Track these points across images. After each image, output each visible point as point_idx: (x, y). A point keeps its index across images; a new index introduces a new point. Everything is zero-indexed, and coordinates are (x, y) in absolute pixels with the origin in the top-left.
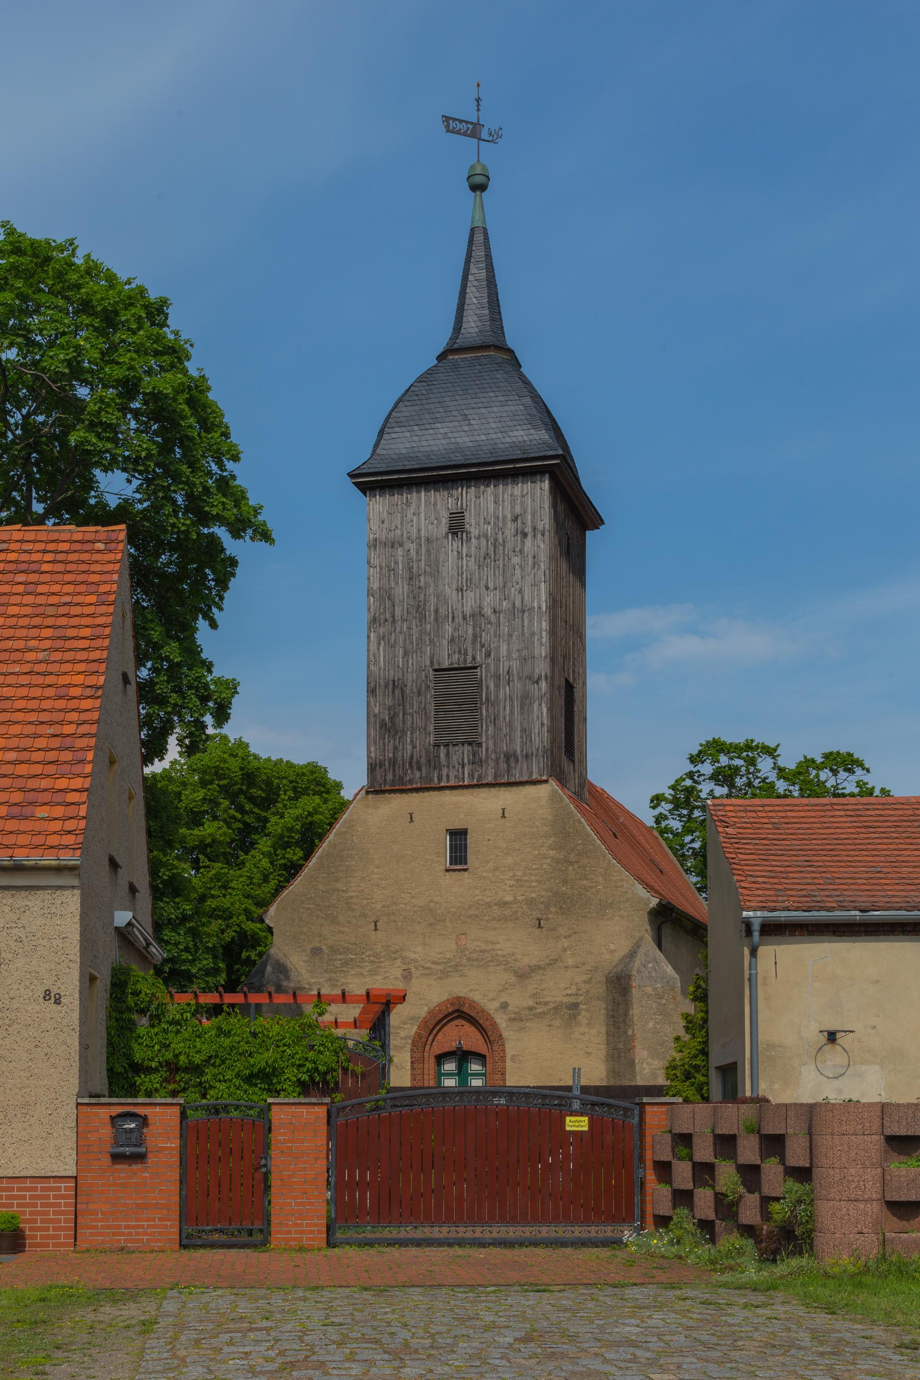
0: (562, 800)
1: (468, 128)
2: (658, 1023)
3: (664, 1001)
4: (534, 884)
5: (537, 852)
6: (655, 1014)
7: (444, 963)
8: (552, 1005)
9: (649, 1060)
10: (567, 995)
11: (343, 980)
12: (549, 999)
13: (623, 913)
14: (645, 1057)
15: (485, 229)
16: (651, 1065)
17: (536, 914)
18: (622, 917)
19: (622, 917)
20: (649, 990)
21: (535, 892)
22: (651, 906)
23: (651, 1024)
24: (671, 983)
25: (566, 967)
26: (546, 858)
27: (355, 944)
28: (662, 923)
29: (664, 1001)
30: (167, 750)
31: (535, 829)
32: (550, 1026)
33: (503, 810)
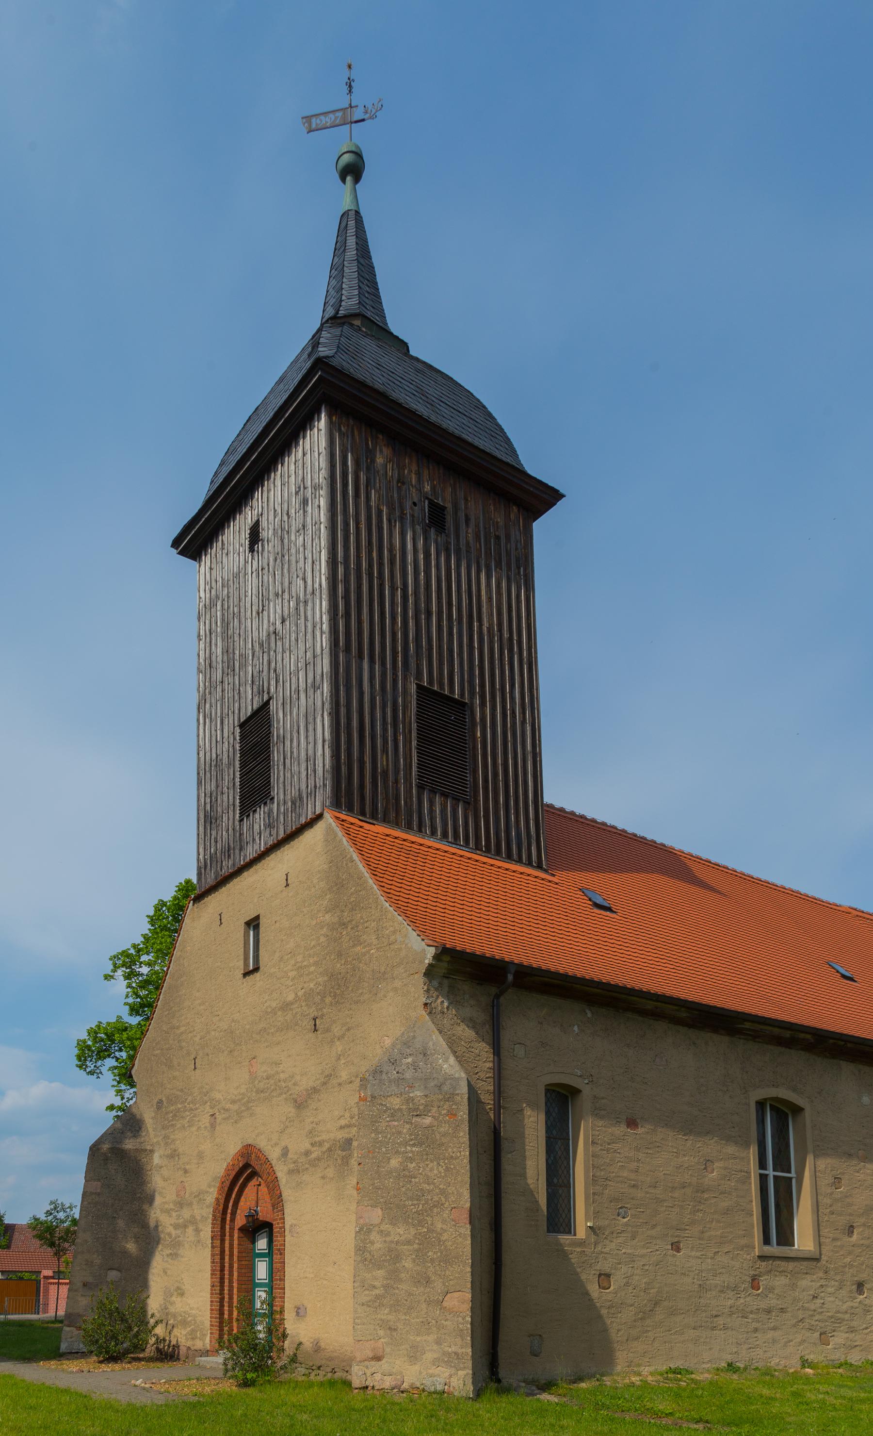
0: (336, 835)
1: (336, 118)
2: (411, 1160)
3: (428, 1121)
4: (312, 969)
5: (314, 922)
6: (406, 1144)
7: (239, 1100)
8: (327, 1145)
9: (385, 1227)
10: (341, 1128)
11: (172, 1137)
12: (324, 1137)
13: (398, 984)
14: (376, 1221)
15: (357, 213)
16: (388, 1234)
17: (313, 1012)
18: (395, 990)
19: (395, 990)
20: (396, 1102)
21: (311, 980)
22: (427, 961)
23: (394, 1163)
24: (446, 1088)
25: (340, 1084)
26: (322, 928)
27: (182, 1091)
28: (497, 997)
29: (428, 1121)
30: (152, 920)
31: (313, 890)
32: (323, 1178)
33: (287, 875)
